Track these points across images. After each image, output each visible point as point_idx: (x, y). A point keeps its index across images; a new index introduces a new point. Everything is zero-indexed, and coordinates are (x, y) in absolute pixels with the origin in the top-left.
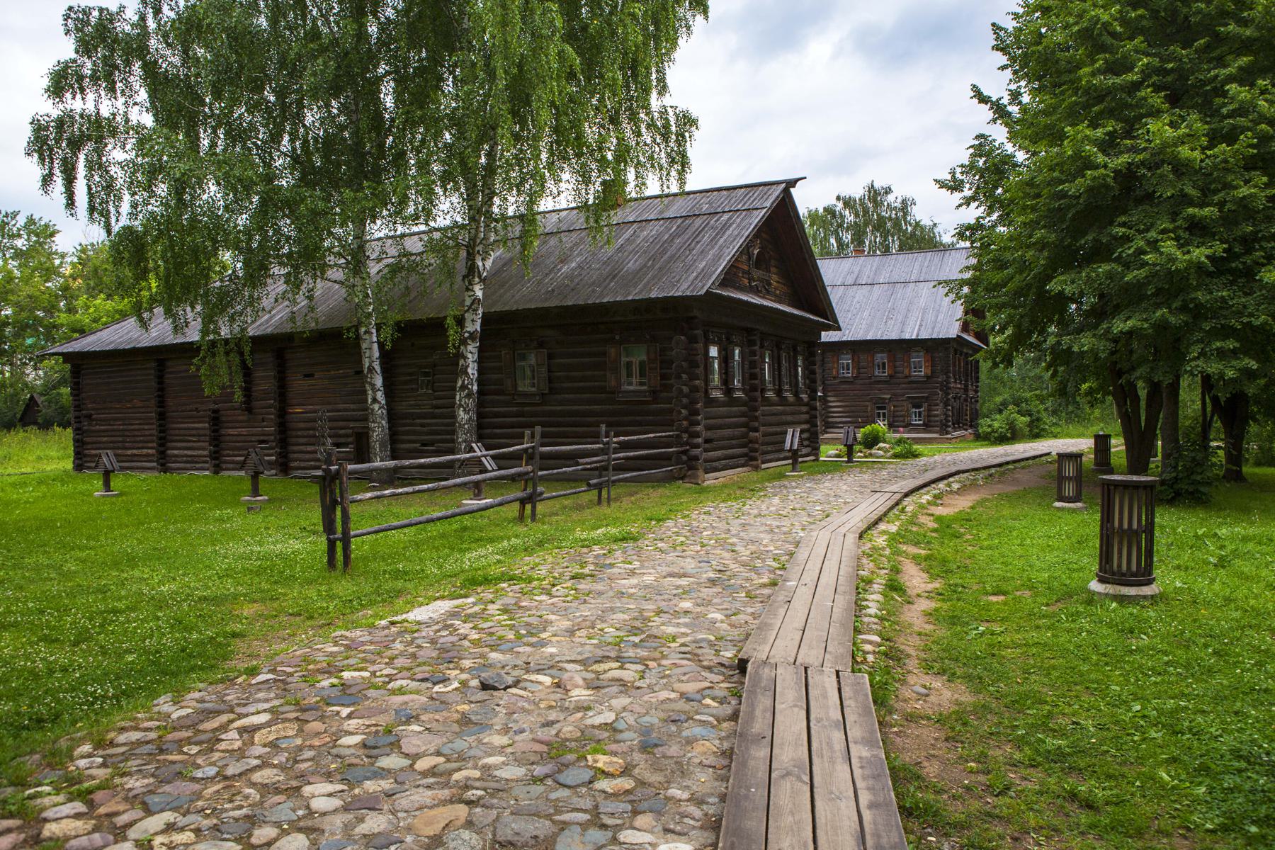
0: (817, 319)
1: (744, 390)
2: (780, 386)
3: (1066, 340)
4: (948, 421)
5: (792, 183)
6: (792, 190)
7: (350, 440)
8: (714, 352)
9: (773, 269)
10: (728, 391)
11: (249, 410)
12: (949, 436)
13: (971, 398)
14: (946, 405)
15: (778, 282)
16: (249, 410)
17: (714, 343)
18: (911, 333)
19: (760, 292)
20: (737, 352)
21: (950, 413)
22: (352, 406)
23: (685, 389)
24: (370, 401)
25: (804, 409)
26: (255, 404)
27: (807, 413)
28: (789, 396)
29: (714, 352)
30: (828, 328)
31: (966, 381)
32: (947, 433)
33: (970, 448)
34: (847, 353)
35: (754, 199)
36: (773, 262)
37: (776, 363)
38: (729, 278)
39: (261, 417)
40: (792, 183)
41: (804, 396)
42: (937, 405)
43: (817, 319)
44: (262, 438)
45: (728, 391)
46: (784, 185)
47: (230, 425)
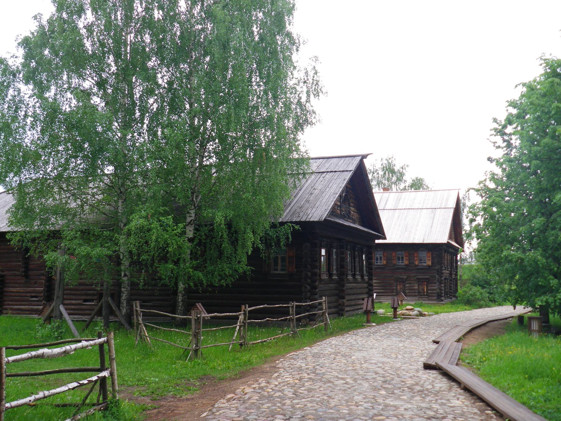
0: (375, 233)
1: (337, 275)
2: (355, 272)
3: (552, 264)
4: (442, 293)
5: (364, 157)
6: (364, 160)
7: (95, 297)
8: (323, 252)
9: (352, 204)
10: (330, 275)
11: (27, 276)
12: (443, 302)
13: (454, 279)
14: (441, 283)
15: (354, 211)
16: (27, 276)
17: (324, 248)
18: (417, 240)
19: (345, 217)
20: (364, 256)
21: (443, 288)
22: (382, 291)
23: (309, 274)
24: (123, 275)
25: (366, 285)
26: (31, 273)
27: (367, 288)
28: (358, 277)
29: (323, 252)
30: (379, 238)
31: (451, 269)
32: (442, 301)
33: (466, 310)
34: (380, 250)
35: (342, 165)
36: (351, 200)
37: (353, 257)
38: (333, 212)
39: (35, 281)
40: (364, 157)
41: (366, 278)
42: (435, 283)
43: (375, 233)
44: (33, 294)
45: (330, 275)
46: (359, 158)
47: (11, 285)
